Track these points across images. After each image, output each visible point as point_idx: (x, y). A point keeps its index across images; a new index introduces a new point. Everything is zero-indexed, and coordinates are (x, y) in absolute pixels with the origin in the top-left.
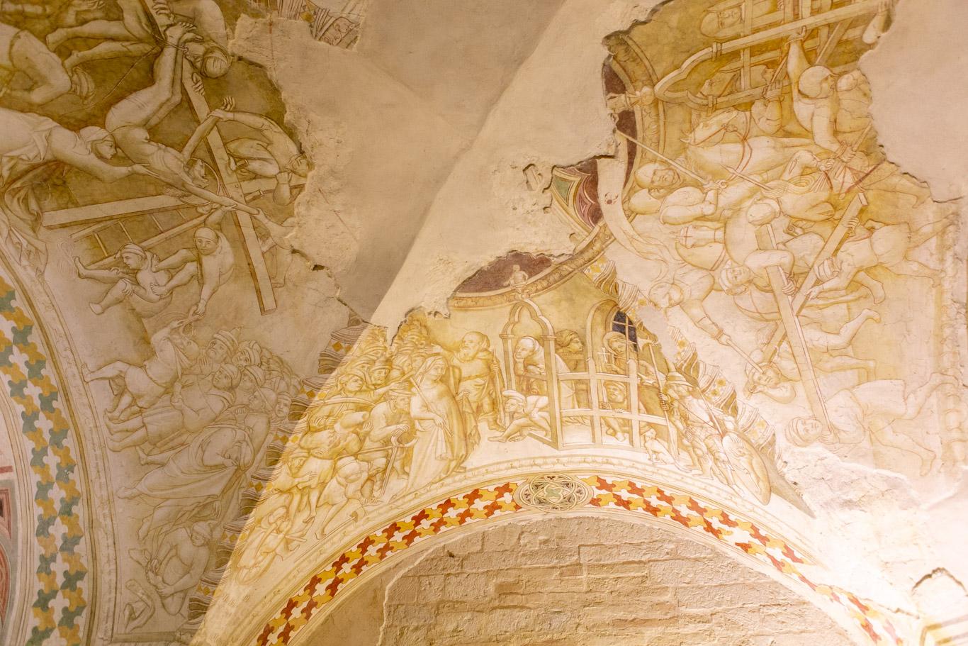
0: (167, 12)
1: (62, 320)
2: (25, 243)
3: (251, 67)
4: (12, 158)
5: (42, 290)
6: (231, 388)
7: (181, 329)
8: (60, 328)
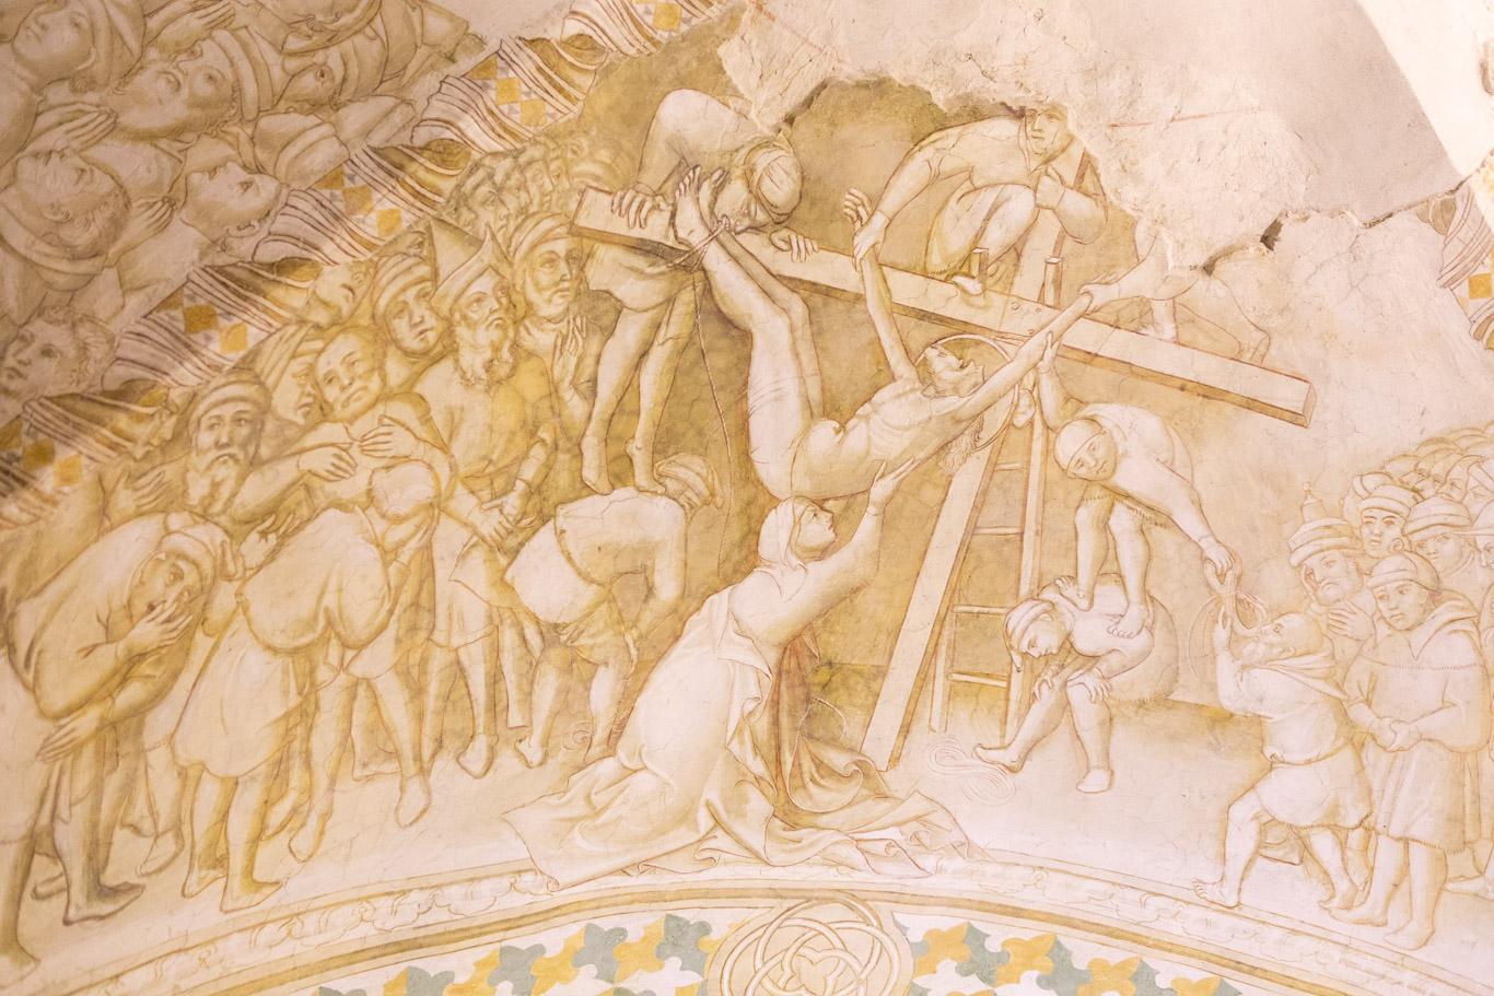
0: (648, 205)
1: (1082, 871)
2: (893, 834)
3: (815, 106)
4: (739, 731)
5: (999, 869)
6: (1435, 594)
7: (1239, 628)
8: (1090, 885)
